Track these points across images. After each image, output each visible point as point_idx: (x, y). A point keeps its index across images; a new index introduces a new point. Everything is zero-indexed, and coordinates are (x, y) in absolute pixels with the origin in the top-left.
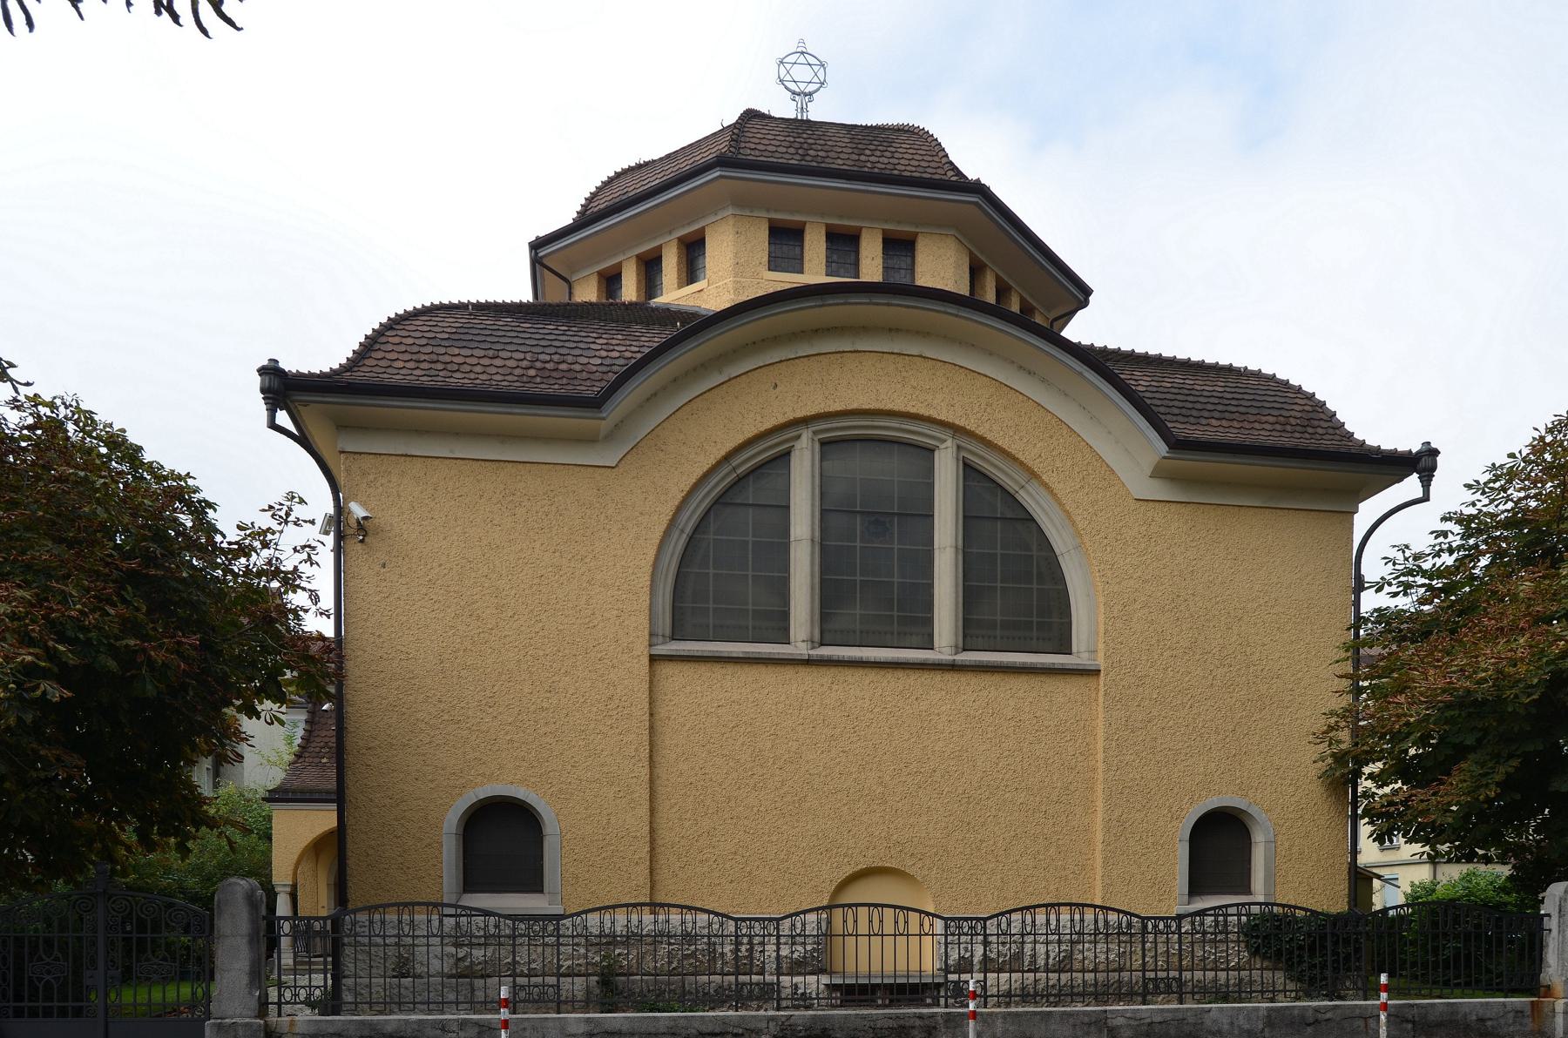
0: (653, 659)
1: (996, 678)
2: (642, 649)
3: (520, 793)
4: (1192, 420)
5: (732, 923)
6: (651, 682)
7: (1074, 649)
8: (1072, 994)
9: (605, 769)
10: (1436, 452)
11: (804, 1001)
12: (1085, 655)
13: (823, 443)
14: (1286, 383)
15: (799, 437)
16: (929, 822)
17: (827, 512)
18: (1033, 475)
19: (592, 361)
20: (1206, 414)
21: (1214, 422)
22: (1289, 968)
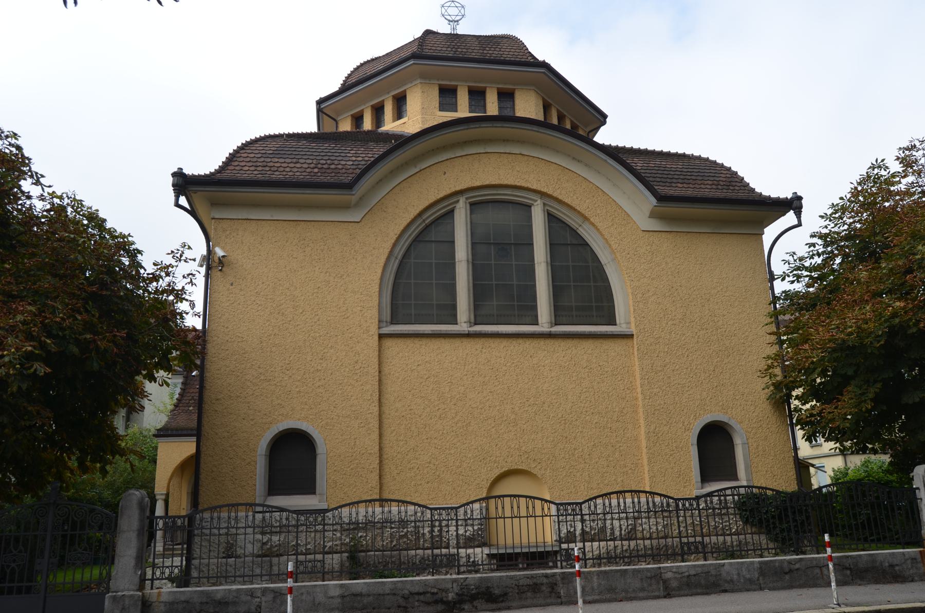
0: (381, 336)
1: (575, 342)
2: (374, 331)
6: (380, 351)
7: (540, 322)
8: (638, 556)
10: (800, 198)
11: (473, 567)
12: (624, 326)
15: (458, 201)
17: (475, 244)
18: (586, 219)
20: (674, 181)
21: (679, 185)
22: (768, 533)
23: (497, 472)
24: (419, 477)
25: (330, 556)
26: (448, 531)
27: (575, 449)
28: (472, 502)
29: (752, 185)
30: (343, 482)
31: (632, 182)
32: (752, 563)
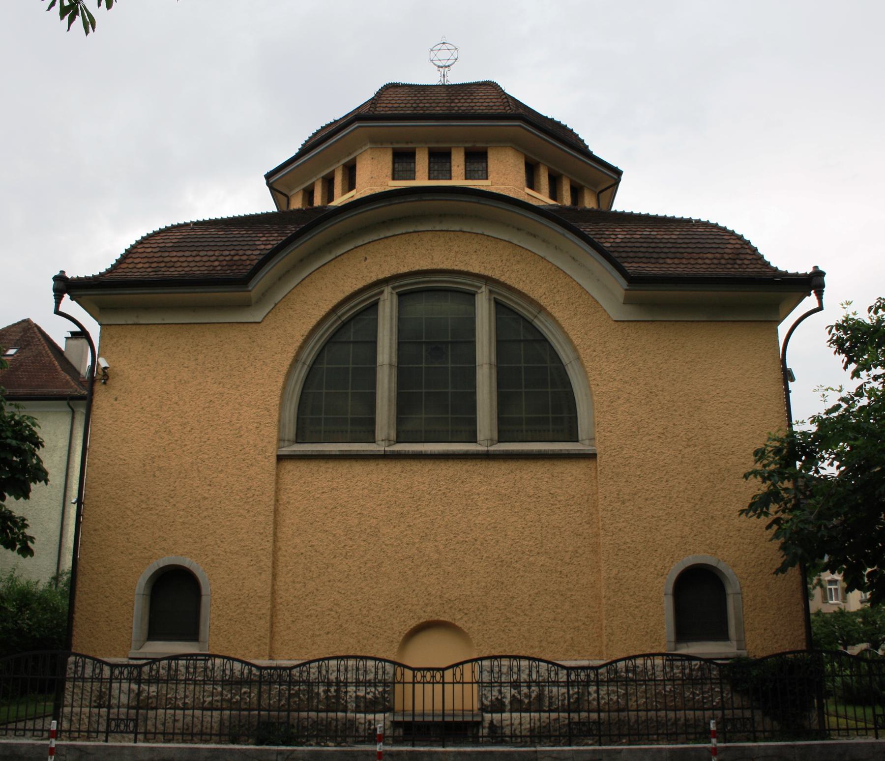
0: (280, 458)
2: (272, 452)
3: (187, 562)
4: (653, 260)
5: (411, 672)
7: (580, 438)
9: (243, 544)
10: (822, 274)
11: (373, 737)
12: (587, 442)
13: (400, 295)
14: (724, 229)
15: (382, 292)
16: (472, 582)
17: (403, 343)
18: (541, 309)
19: (255, 253)
20: (663, 256)
21: (669, 261)
23: (413, 623)
24: (317, 627)
25: (209, 713)
26: (346, 692)
27: (513, 598)
28: (482, 659)
29: (766, 258)
30: (231, 631)
31: (588, 253)
32: (660, 751)
